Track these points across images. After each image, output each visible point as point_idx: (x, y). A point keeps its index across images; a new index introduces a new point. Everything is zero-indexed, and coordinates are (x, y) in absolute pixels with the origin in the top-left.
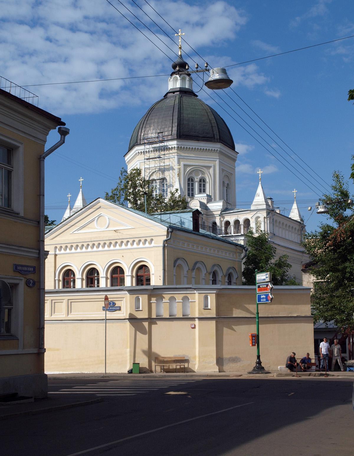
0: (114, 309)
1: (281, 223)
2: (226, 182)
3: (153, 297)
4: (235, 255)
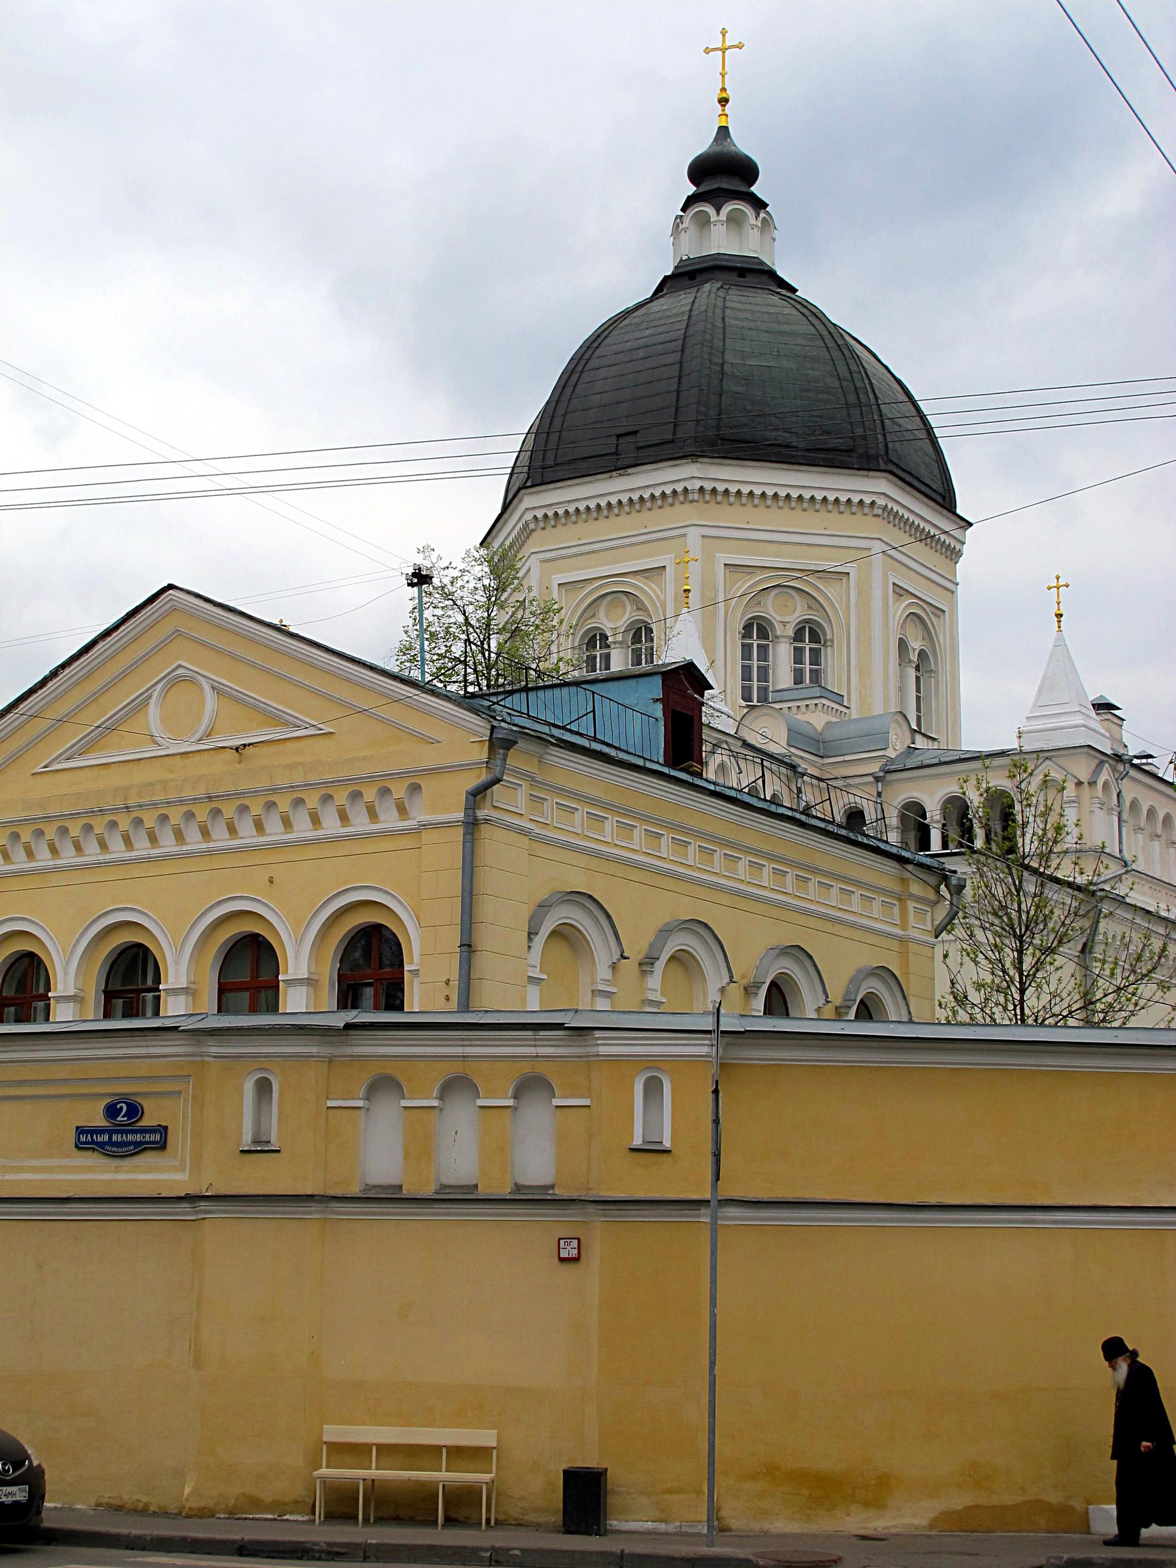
0: (136, 1144)
1: (1161, 815)
2: (916, 645)
4: (896, 910)
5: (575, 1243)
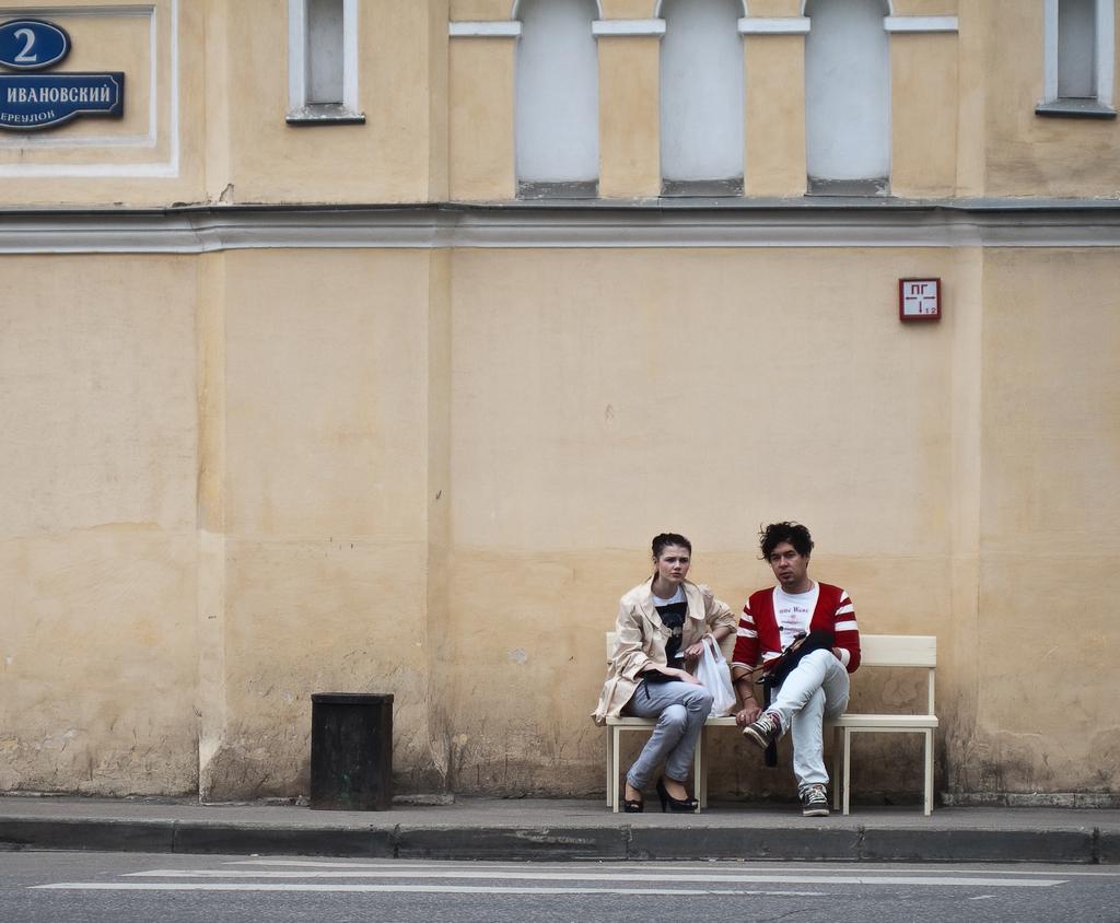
0: (61, 109)
3: (834, 627)
5: (931, 289)
